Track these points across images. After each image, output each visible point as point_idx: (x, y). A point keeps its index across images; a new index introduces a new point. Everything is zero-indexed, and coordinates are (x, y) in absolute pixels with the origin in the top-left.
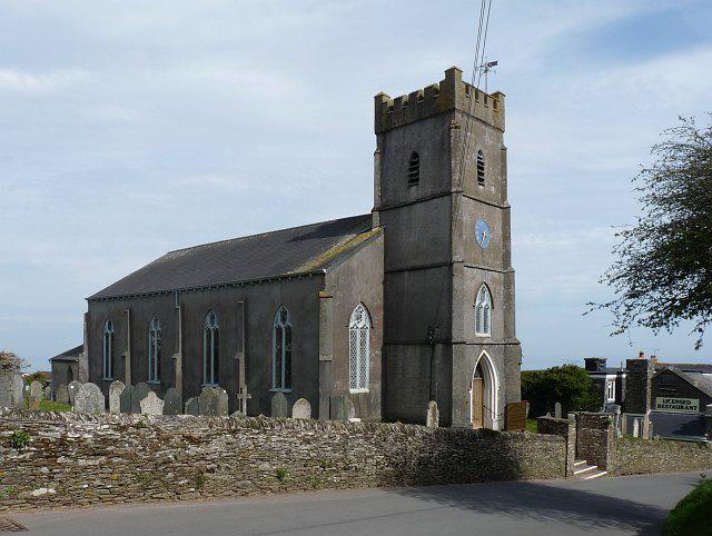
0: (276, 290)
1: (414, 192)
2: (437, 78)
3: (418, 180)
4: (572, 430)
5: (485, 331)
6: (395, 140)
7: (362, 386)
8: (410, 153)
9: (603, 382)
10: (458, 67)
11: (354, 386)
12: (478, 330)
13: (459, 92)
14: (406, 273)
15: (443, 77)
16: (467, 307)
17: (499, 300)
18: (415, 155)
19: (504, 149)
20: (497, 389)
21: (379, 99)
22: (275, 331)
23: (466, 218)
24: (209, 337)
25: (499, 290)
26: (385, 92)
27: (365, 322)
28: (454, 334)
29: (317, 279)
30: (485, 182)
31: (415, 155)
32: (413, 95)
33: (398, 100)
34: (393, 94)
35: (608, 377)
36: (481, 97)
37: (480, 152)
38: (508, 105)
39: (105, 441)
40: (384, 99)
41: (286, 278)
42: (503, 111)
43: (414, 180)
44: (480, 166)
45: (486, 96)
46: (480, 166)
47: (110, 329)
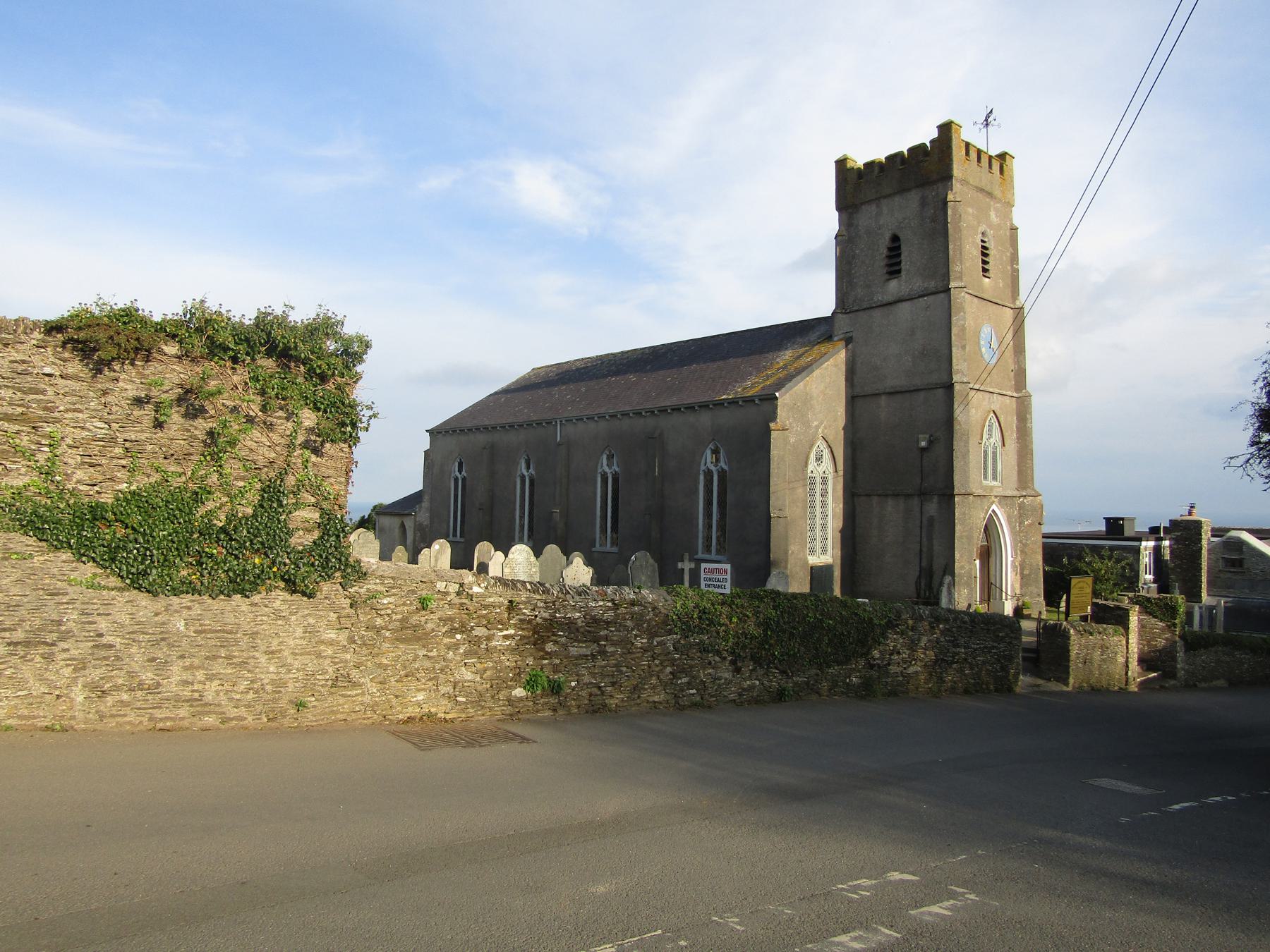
0: (705, 419)
1: (894, 287)
2: (926, 134)
3: (899, 271)
4: (1134, 620)
5: (995, 478)
6: (865, 218)
7: (824, 551)
8: (888, 236)
9: (1137, 551)
10: (956, 121)
11: (812, 551)
12: (985, 478)
13: (958, 153)
14: (883, 397)
15: (935, 134)
16: (973, 442)
17: (1012, 437)
18: (895, 238)
19: (1014, 229)
20: (1010, 559)
21: (841, 164)
22: (702, 477)
23: (970, 323)
24: (995, 469)
25: (1011, 422)
26: (850, 155)
27: (827, 464)
28: (956, 483)
29: (766, 406)
30: (991, 274)
31: (895, 238)
32: (891, 158)
33: (869, 165)
34: (860, 159)
35: (1144, 543)
36: (974, 155)
37: (209, 292)
38: (1019, 169)
39: (595, 621)
40: (850, 165)
41: (720, 404)
42: (1012, 178)
43: (894, 270)
44: (984, 252)
45: (990, 157)
46: (984, 252)
47: (460, 471)
